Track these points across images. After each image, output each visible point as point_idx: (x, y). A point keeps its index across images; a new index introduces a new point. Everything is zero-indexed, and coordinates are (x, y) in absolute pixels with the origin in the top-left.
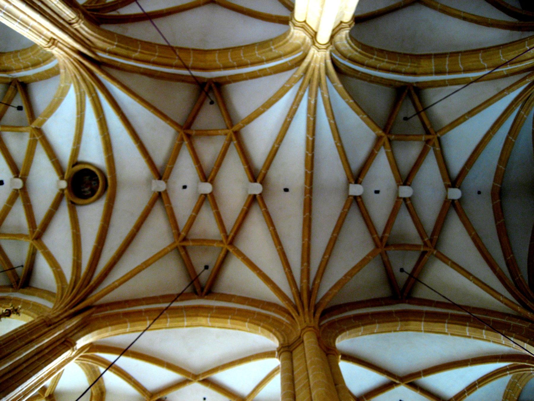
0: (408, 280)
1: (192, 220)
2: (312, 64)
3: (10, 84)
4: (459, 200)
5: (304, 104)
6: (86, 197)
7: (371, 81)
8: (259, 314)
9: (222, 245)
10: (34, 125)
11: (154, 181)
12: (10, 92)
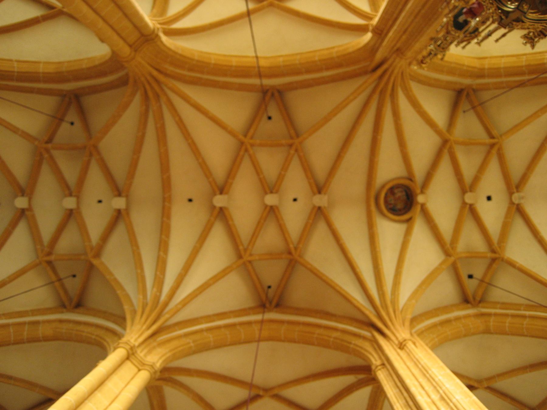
0: (64, 115)
1: (285, 167)
2: (144, 327)
3: (480, 302)
4: (16, 196)
5: (166, 289)
6: (398, 186)
7: (105, 312)
8: (202, 72)
9: (251, 141)
10: (452, 259)
11: (326, 205)
12: (480, 293)
